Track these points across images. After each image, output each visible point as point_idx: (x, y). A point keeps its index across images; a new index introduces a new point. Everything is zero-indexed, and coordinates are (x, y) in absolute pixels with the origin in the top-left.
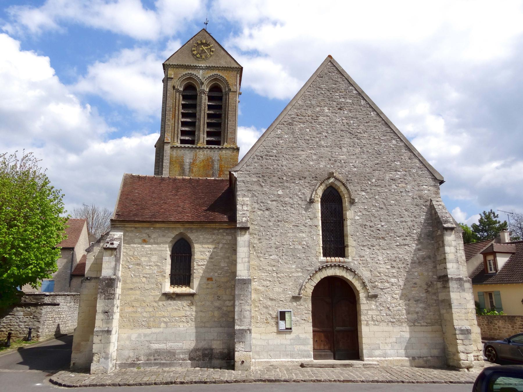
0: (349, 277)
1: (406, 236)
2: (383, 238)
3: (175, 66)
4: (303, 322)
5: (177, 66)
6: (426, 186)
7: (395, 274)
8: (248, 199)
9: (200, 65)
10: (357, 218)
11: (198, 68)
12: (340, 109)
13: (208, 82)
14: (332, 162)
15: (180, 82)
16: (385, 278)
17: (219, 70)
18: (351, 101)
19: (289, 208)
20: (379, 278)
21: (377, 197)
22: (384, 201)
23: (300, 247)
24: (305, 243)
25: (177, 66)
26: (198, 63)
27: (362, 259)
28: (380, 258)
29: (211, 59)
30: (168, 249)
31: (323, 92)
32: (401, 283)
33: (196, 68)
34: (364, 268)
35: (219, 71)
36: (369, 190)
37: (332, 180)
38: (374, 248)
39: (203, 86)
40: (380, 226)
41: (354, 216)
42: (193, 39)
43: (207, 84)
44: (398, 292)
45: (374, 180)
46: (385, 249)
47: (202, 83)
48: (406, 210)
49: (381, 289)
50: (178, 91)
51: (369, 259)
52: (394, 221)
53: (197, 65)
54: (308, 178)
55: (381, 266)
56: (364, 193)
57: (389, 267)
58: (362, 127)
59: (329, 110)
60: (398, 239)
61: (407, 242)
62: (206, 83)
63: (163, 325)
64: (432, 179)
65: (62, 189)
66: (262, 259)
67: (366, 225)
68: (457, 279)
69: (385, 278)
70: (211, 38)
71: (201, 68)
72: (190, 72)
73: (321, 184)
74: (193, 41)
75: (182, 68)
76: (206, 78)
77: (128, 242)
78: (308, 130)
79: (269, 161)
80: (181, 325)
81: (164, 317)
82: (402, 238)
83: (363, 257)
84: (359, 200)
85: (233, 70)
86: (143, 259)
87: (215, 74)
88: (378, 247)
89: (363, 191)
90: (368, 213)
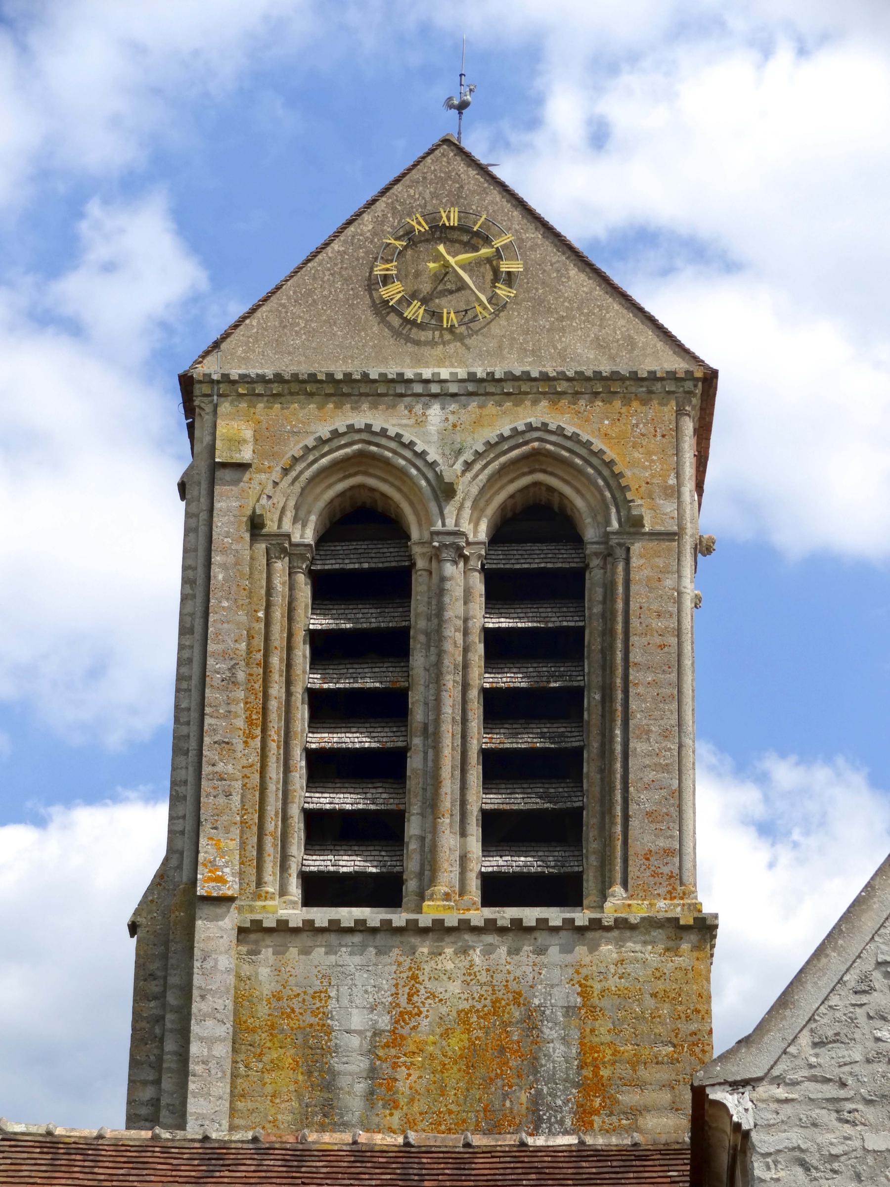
3: (259, 389)
5: (276, 388)
9: (427, 374)
11: (418, 388)
15: (297, 488)
17: (555, 396)
26: (418, 361)
35: (554, 403)
39: (450, 510)
43: (474, 490)
47: (445, 491)
53: (409, 374)
74: (380, 222)
76: (468, 456)
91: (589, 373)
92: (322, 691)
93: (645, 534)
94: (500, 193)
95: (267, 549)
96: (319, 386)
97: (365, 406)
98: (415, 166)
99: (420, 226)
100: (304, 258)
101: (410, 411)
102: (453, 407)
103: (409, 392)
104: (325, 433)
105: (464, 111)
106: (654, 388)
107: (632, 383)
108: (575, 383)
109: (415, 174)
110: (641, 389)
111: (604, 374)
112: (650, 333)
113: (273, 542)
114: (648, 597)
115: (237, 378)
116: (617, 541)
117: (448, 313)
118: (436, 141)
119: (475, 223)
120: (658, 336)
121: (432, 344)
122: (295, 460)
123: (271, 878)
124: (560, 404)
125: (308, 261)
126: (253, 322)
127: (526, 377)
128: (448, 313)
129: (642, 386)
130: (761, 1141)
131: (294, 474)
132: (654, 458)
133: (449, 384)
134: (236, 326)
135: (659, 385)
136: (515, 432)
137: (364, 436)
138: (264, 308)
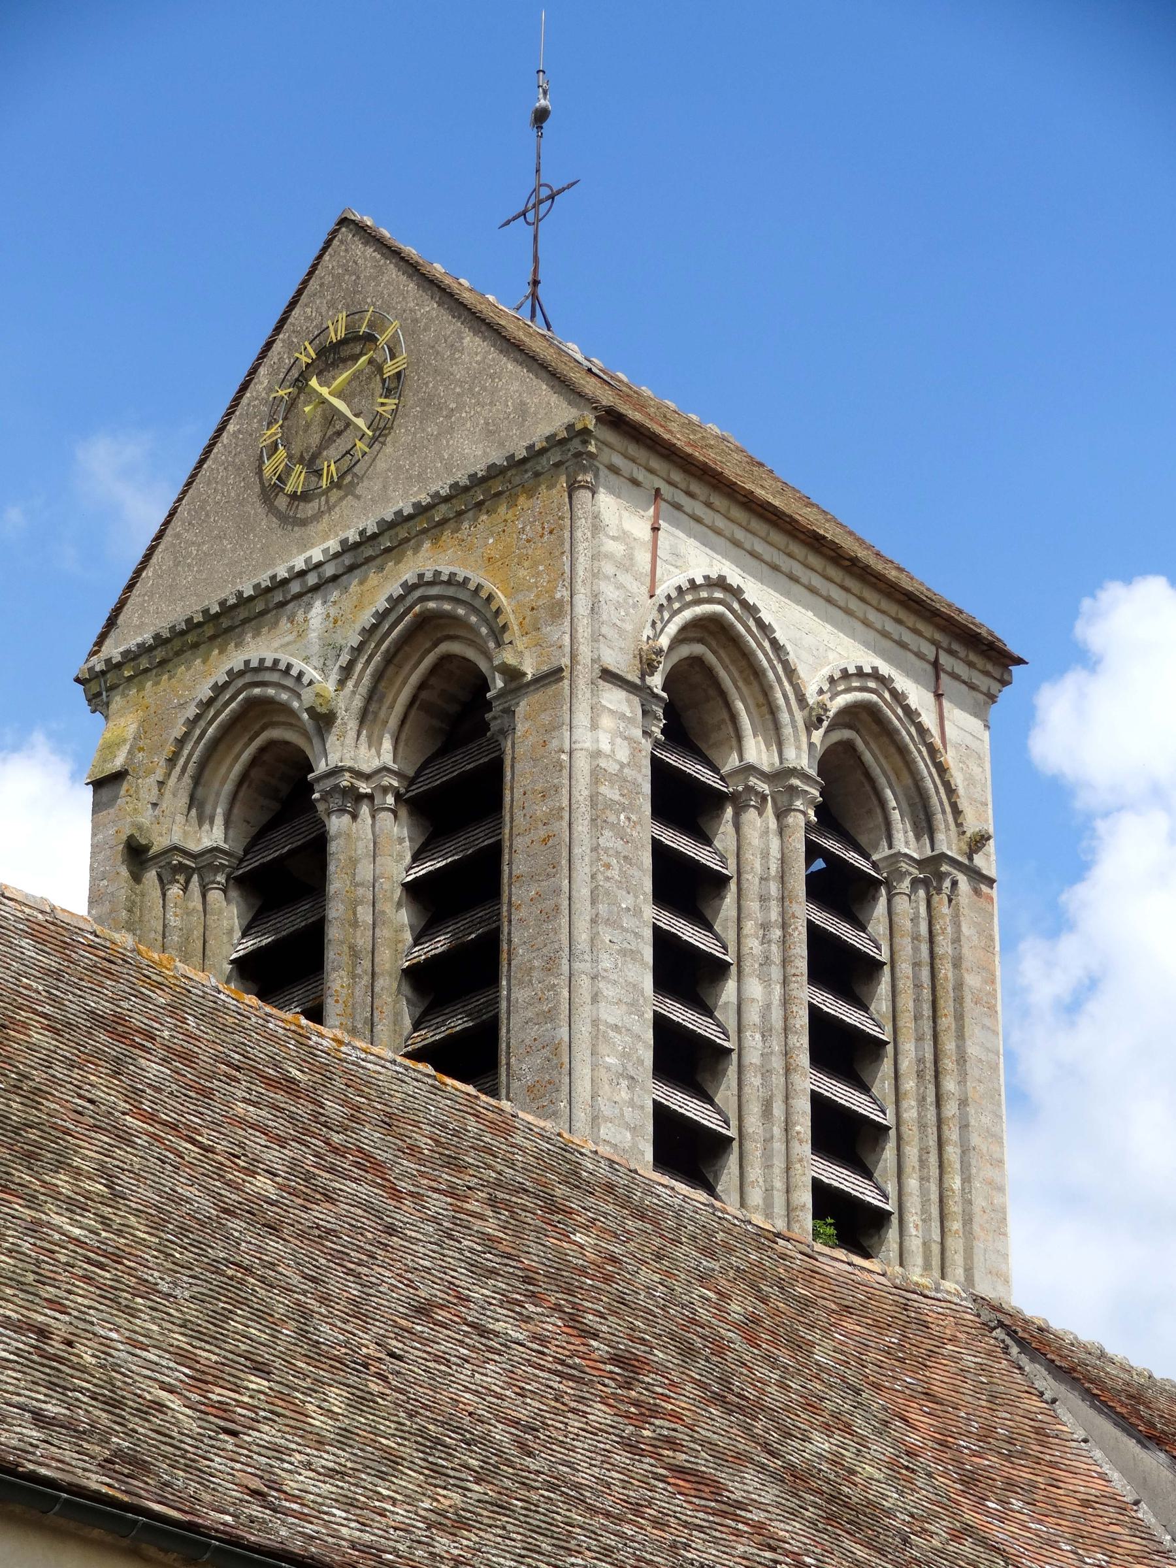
3: (144, 663)
5: (159, 654)
9: (299, 564)
11: (295, 587)
13: (366, 680)
15: (187, 780)
25: (159, 654)
26: (304, 546)
33: (278, 597)
39: (331, 740)
42: (278, 346)
43: (358, 702)
47: (324, 720)
53: (282, 573)
65: (529, 117)
70: (392, 272)
71: (312, 579)
72: (235, 659)
74: (274, 372)
75: (195, 646)
76: (345, 658)
85: (537, 475)
87: (409, 588)
91: (464, 481)
92: (433, 962)
93: (529, 684)
94: (396, 265)
95: (159, 876)
96: (199, 630)
97: (248, 637)
98: (311, 273)
100: (197, 459)
101: (292, 622)
102: (335, 595)
103: (289, 597)
104: (205, 693)
105: (544, 125)
106: (539, 468)
107: (513, 472)
108: (454, 501)
109: (313, 285)
110: (526, 476)
111: (480, 474)
112: (544, 387)
113: (163, 863)
114: (532, 773)
115: (119, 659)
116: (501, 707)
117: (329, 466)
118: (332, 226)
119: (360, 327)
120: (553, 387)
121: (317, 517)
122: (181, 742)
123: (610, 1014)
124: (444, 538)
125: (202, 462)
126: (148, 573)
127: (401, 519)
128: (329, 466)
129: (526, 471)
131: (182, 761)
132: (541, 568)
133: (326, 567)
134: (130, 587)
135: (544, 461)
136: (394, 601)
137: (248, 678)
138: (160, 548)
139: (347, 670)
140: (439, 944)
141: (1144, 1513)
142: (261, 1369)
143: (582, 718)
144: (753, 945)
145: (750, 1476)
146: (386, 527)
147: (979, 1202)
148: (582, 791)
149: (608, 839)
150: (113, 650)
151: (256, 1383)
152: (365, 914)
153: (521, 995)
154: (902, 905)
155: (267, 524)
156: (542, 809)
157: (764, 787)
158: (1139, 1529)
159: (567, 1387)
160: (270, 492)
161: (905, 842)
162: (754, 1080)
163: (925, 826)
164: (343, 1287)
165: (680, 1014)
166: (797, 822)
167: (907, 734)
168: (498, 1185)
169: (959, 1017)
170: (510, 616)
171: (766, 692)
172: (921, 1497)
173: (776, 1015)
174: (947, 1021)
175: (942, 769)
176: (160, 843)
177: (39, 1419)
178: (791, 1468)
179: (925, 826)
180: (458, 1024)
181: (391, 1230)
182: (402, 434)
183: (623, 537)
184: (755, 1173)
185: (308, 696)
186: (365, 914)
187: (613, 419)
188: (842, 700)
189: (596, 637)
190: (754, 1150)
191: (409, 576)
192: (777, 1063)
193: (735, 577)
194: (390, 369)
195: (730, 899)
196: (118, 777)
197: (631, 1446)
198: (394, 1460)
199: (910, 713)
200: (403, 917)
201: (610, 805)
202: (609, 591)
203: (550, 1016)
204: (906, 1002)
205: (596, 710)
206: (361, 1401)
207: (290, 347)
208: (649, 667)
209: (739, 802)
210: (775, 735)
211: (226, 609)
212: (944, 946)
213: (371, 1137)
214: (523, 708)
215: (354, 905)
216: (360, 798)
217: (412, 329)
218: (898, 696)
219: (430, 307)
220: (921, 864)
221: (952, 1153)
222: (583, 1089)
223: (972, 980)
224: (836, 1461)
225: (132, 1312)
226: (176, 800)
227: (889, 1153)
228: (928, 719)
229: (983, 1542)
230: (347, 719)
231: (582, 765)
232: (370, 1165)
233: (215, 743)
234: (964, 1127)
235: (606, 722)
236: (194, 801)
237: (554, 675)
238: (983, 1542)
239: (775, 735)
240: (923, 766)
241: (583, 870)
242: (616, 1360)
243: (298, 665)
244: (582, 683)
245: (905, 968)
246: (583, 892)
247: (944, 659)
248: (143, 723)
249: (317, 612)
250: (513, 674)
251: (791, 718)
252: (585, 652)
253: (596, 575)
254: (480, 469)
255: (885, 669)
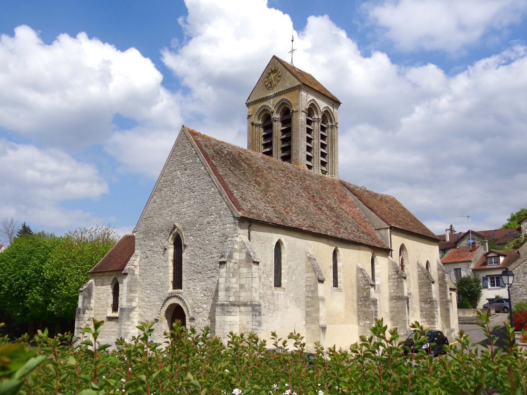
0: (181, 305)
1: (214, 270)
2: (200, 272)
4: (159, 337)
6: (229, 224)
7: (206, 301)
8: (138, 251)
10: (188, 258)
12: (186, 170)
14: (178, 215)
16: (200, 304)
17: (284, 93)
18: (191, 161)
19: (156, 255)
20: (197, 304)
21: (198, 239)
22: (202, 242)
23: (159, 283)
24: (161, 280)
26: (270, 93)
27: (188, 290)
28: (198, 289)
29: (279, 84)
30: (110, 288)
31: (178, 158)
32: (209, 309)
34: (189, 297)
36: (194, 235)
37: (176, 230)
38: (195, 281)
40: (199, 263)
41: (186, 257)
44: (207, 315)
45: (197, 226)
46: (201, 281)
47: (273, 112)
48: (215, 248)
49: (198, 313)
50: (257, 125)
51: (192, 290)
52: (207, 258)
54: (165, 231)
55: (198, 295)
56: (192, 238)
57: (202, 296)
58: (196, 182)
59: (180, 172)
60: (209, 272)
61: (213, 275)
62: (275, 111)
63: (106, 336)
64: (233, 217)
66: (143, 293)
67: (191, 263)
68: (221, 304)
69: (200, 304)
73: (170, 234)
77: (96, 285)
78: (168, 192)
79: (149, 221)
80: (113, 337)
81: (107, 332)
82: (211, 271)
83: (189, 288)
84: (189, 243)
86: (102, 295)
88: (197, 280)
89: (191, 235)
90: (193, 253)
99: (270, 71)
123: (303, 147)
130: (136, 238)
136: (280, 101)
139: (275, 107)
140: (284, 136)
141: (355, 202)
142: (288, 206)
143: (300, 116)
144: (315, 137)
145: (324, 207)
146: (279, 92)
147: (336, 161)
148: (300, 124)
149: (303, 129)
150: (249, 101)
151: (288, 208)
152: (277, 133)
153: (293, 144)
154: (329, 130)
155: (266, 89)
156: (296, 125)
157: (316, 120)
158: (354, 204)
159: (309, 200)
160: (266, 86)
161: (330, 124)
162: (315, 151)
163: (331, 122)
164: (292, 194)
165: (309, 145)
166: (320, 124)
167: (330, 113)
168: (300, 177)
169: (334, 142)
170: (293, 104)
171: (317, 110)
172: (336, 206)
173: (317, 144)
174: (333, 143)
175: (333, 116)
176: (255, 123)
177: (277, 218)
178: (327, 205)
179: (331, 122)
180: (287, 145)
181: (293, 186)
182: (281, 82)
183: (304, 96)
184: (315, 160)
185: (271, 110)
186: (277, 133)
187: (303, 84)
188: (324, 110)
189: (301, 107)
190: (315, 158)
191: (282, 98)
192: (317, 149)
193: (315, 99)
194: (279, 74)
195: (313, 132)
196: (250, 116)
197: (315, 206)
198: (299, 214)
199: (331, 110)
200: (281, 133)
201: (303, 125)
202: (303, 102)
203: (297, 147)
204: (329, 140)
205: (301, 115)
206: (296, 207)
207: (268, 70)
208: (306, 110)
209: (314, 121)
210: (318, 114)
211: (262, 99)
212: (333, 135)
213: (290, 175)
214: (294, 114)
215: (276, 132)
216: (276, 120)
217: (281, 70)
218: (329, 109)
219: (283, 68)
220: (331, 126)
221: (333, 156)
222: (300, 154)
223: (336, 138)
224: (330, 203)
225: (279, 203)
226: (257, 118)
227: (327, 156)
228: (332, 111)
229: (342, 209)
230: (275, 112)
231: (300, 121)
232: (291, 178)
233: (260, 113)
234: (335, 153)
235: (302, 116)
236: (258, 118)
237: (297, 111)
238: (342, 209)
239: (318, 114)
240: (332, 116)
241: (300, 132)
242: (312, 196)
243: (270, 106)
244: (300, 112)
245: (329, 137)
246: (300, 134)
247: (334, 104)
248: (253, 110)
249: (272, 100)
250: (293, 111)
251: (319, 113)
252: (300, 109)
253: (301, 100)
254: (289, 88)
255: (328, 106)
